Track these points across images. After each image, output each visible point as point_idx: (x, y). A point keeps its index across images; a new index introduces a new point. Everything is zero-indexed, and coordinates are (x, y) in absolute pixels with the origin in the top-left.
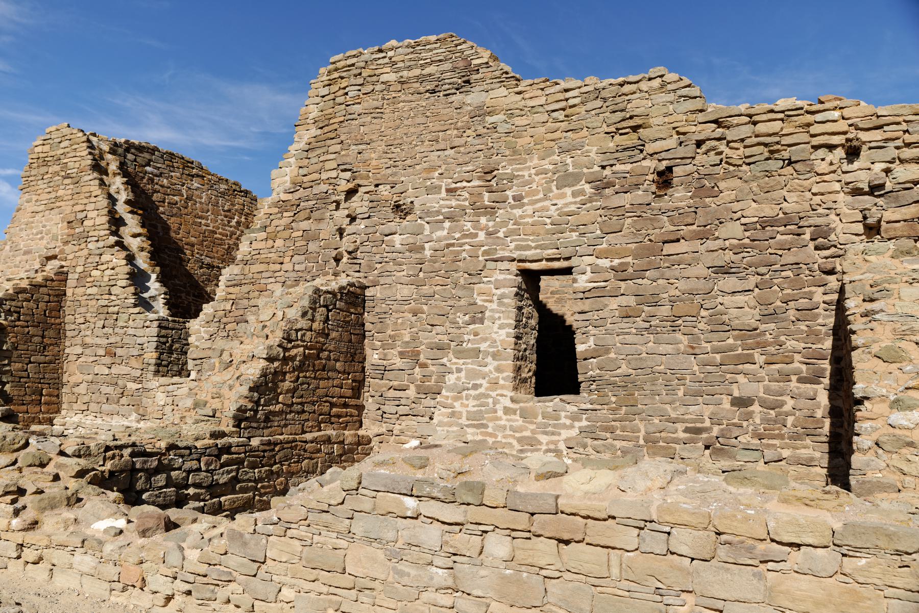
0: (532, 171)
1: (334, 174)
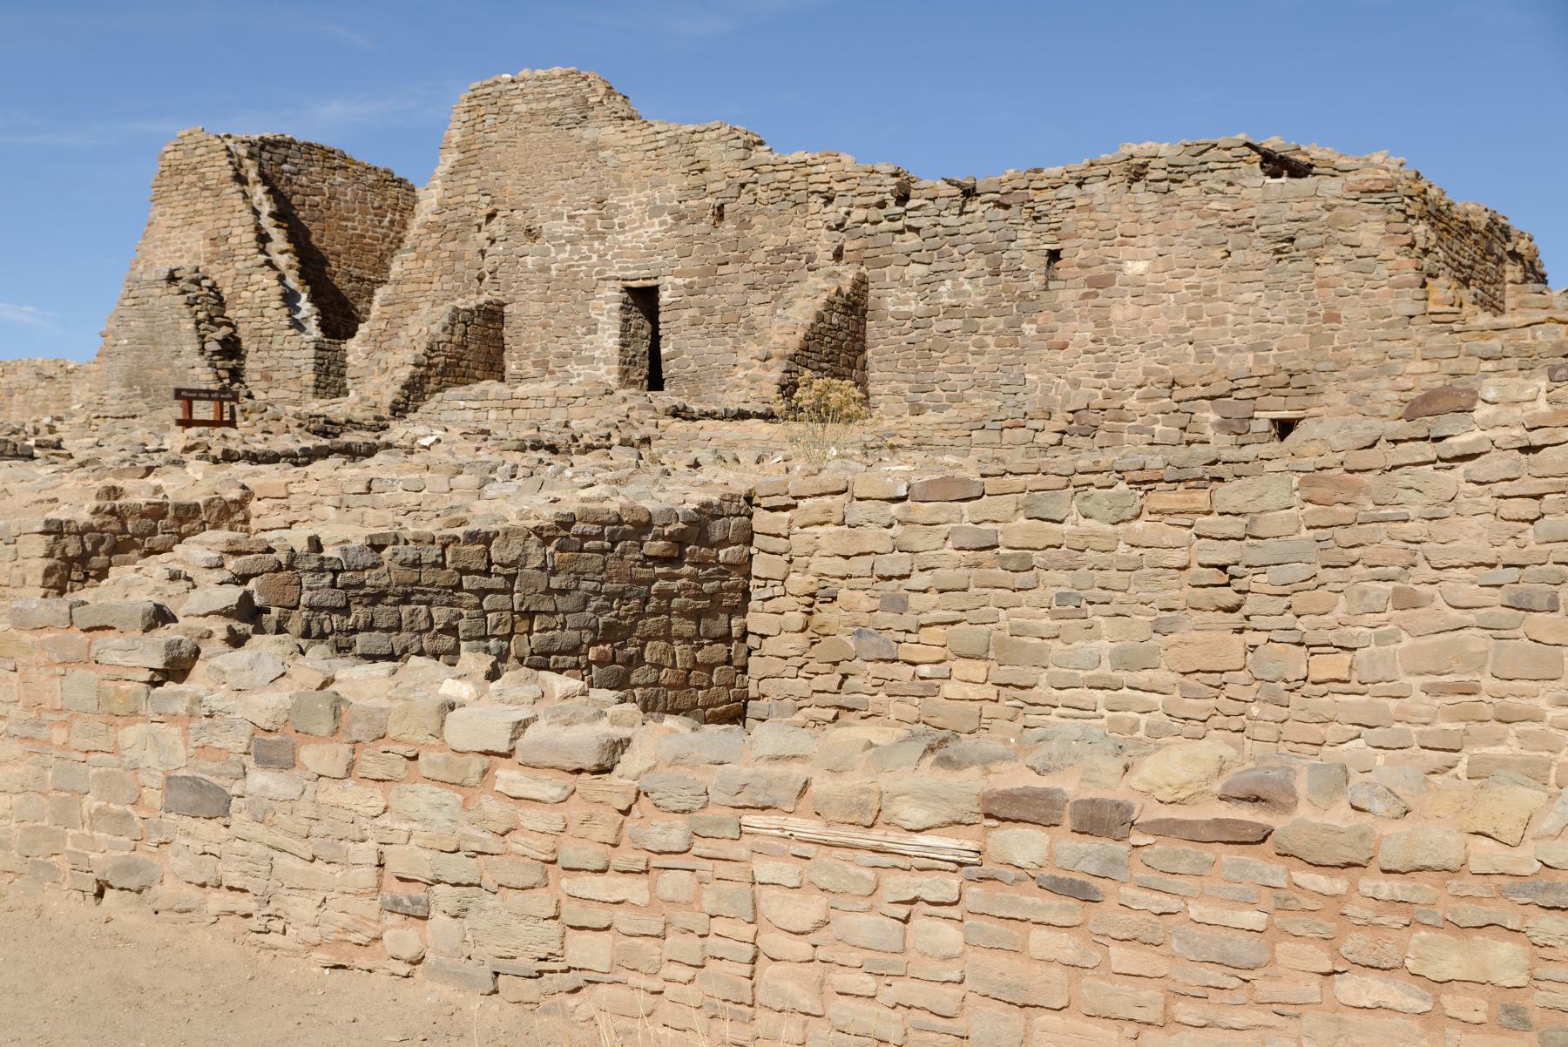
0: (631, 202)
1: (475, 198)
